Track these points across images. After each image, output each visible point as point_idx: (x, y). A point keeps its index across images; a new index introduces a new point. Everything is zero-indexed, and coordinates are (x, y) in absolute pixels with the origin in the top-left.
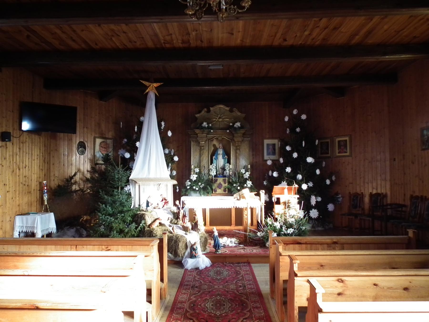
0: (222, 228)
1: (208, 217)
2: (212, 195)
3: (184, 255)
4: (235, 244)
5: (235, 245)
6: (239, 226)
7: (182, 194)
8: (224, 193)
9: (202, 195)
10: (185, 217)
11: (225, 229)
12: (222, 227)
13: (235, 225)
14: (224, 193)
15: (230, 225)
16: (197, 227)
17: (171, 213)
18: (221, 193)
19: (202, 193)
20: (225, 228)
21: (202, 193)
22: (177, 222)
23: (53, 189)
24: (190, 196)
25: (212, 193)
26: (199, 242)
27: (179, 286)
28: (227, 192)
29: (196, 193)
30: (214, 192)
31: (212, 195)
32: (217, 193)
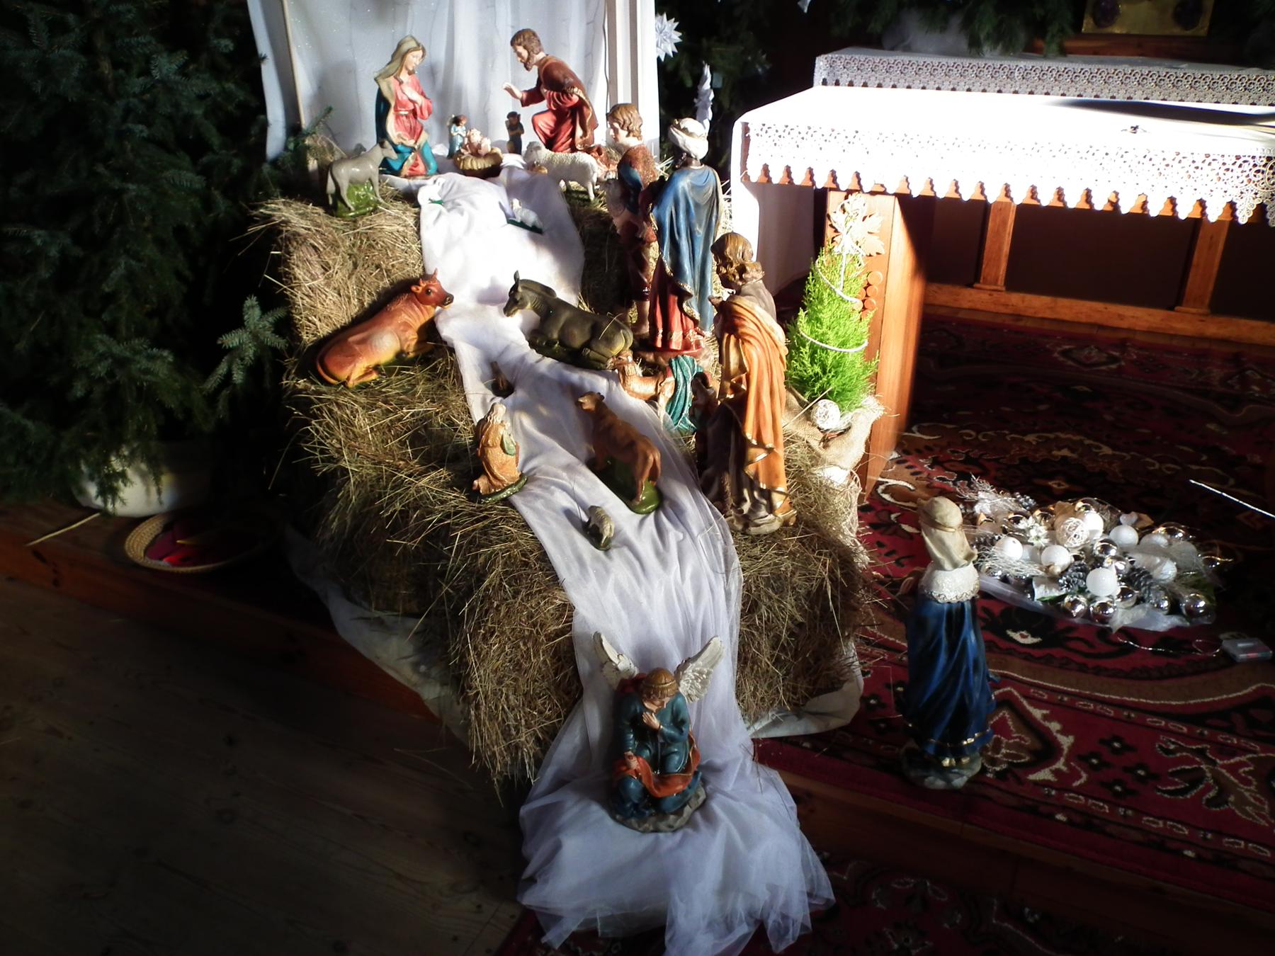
0: (1097, 318)
1: (1004, 223)
2: (1068, 44)
3: (539, 763)
4: (1174, 609)
5: (1165, 623)
6: (1243, 321)
7: (836, 31)
8: (1177, 31)
9: (986, 48)
10: (673, 299)
11: (1124, 324)
12: (1099, 306)
13: (1204, 310)
14: (1177, 31)
15: (1171, 298)
16: (742, 459)
17: (573, 234)
18: (1154, 30)
19: (985, 31)
20: (1121, 317)
21: (988, 28)
22: (587, 345)
23: (956, 21)
24: (893, 49)
25: (1077, 26)
26: (725, 643)
27: (992, 312)
28: (1202, 28)
29: (943, 29)
30: (1088, 25)
31: (1068, 44)
32: (1117, 30)
